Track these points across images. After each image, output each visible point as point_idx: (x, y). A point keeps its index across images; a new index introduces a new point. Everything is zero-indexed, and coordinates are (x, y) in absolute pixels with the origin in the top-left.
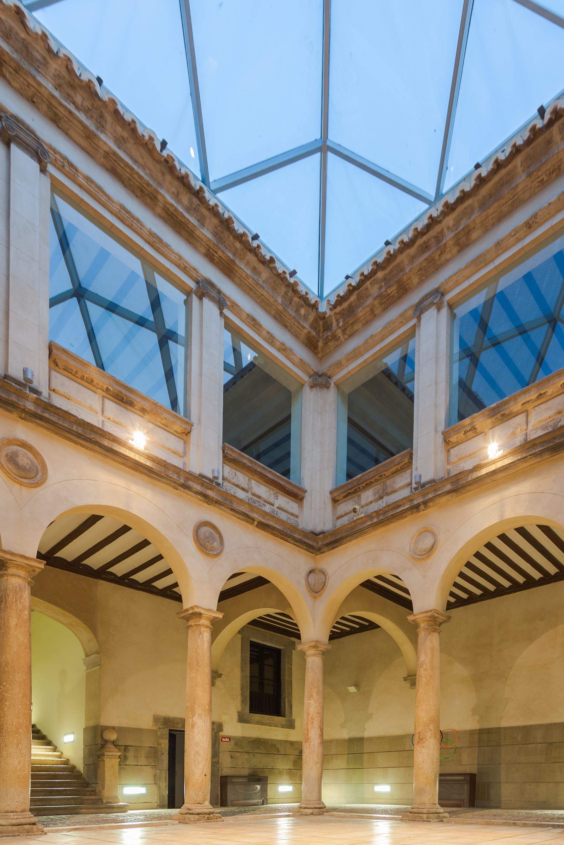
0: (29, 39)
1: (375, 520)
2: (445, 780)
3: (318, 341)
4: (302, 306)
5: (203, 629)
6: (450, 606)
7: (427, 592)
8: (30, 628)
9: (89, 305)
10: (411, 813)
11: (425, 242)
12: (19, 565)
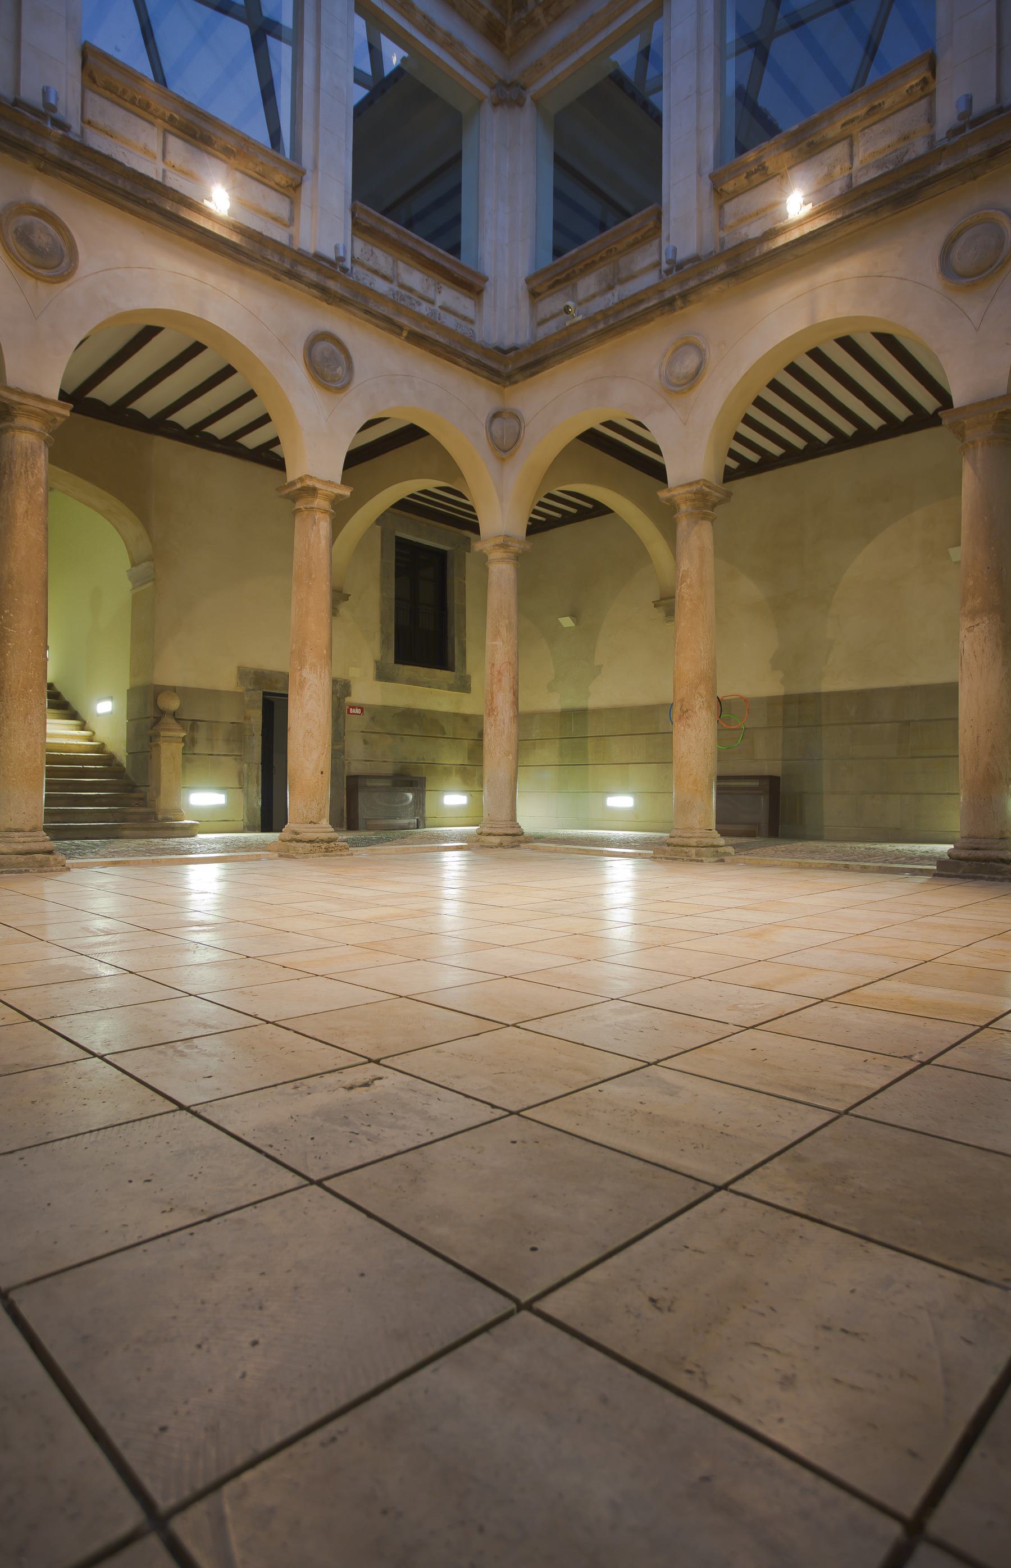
1: (601, 326)
2: (728, 787)
5: (318, 515)
6: (729, 475)
7: (691, 456)
10: (669, 845)
12: (32, 412)
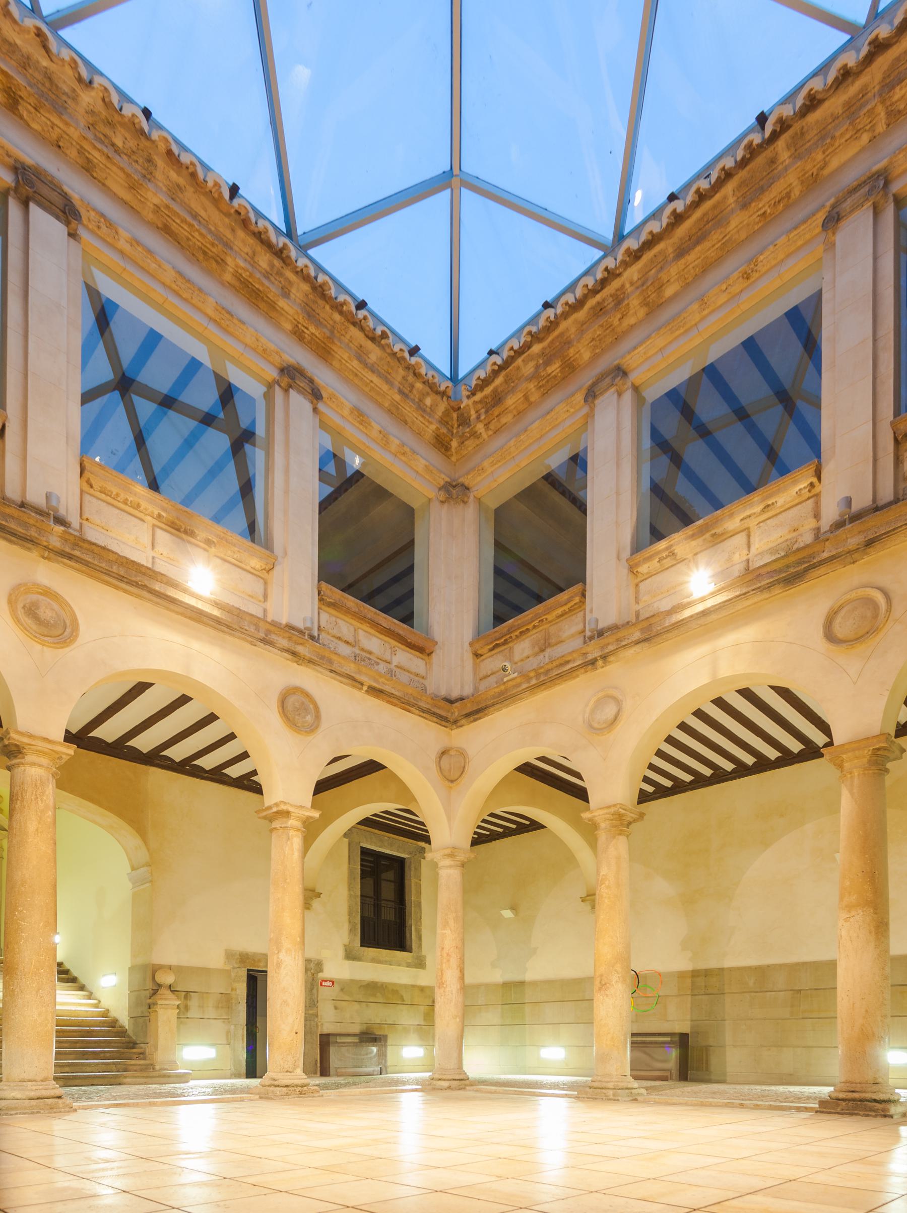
0: (53, 67)
1: (534, 682)
2: (641, 1041)
3: (451, 440)
4: (428, 394)
6: (644, 797)
7: (612, 780)
8: (55, 834)
9: (138, 401)
10: (590, 1088)
11: (598, 303)
12: (40, 751)
